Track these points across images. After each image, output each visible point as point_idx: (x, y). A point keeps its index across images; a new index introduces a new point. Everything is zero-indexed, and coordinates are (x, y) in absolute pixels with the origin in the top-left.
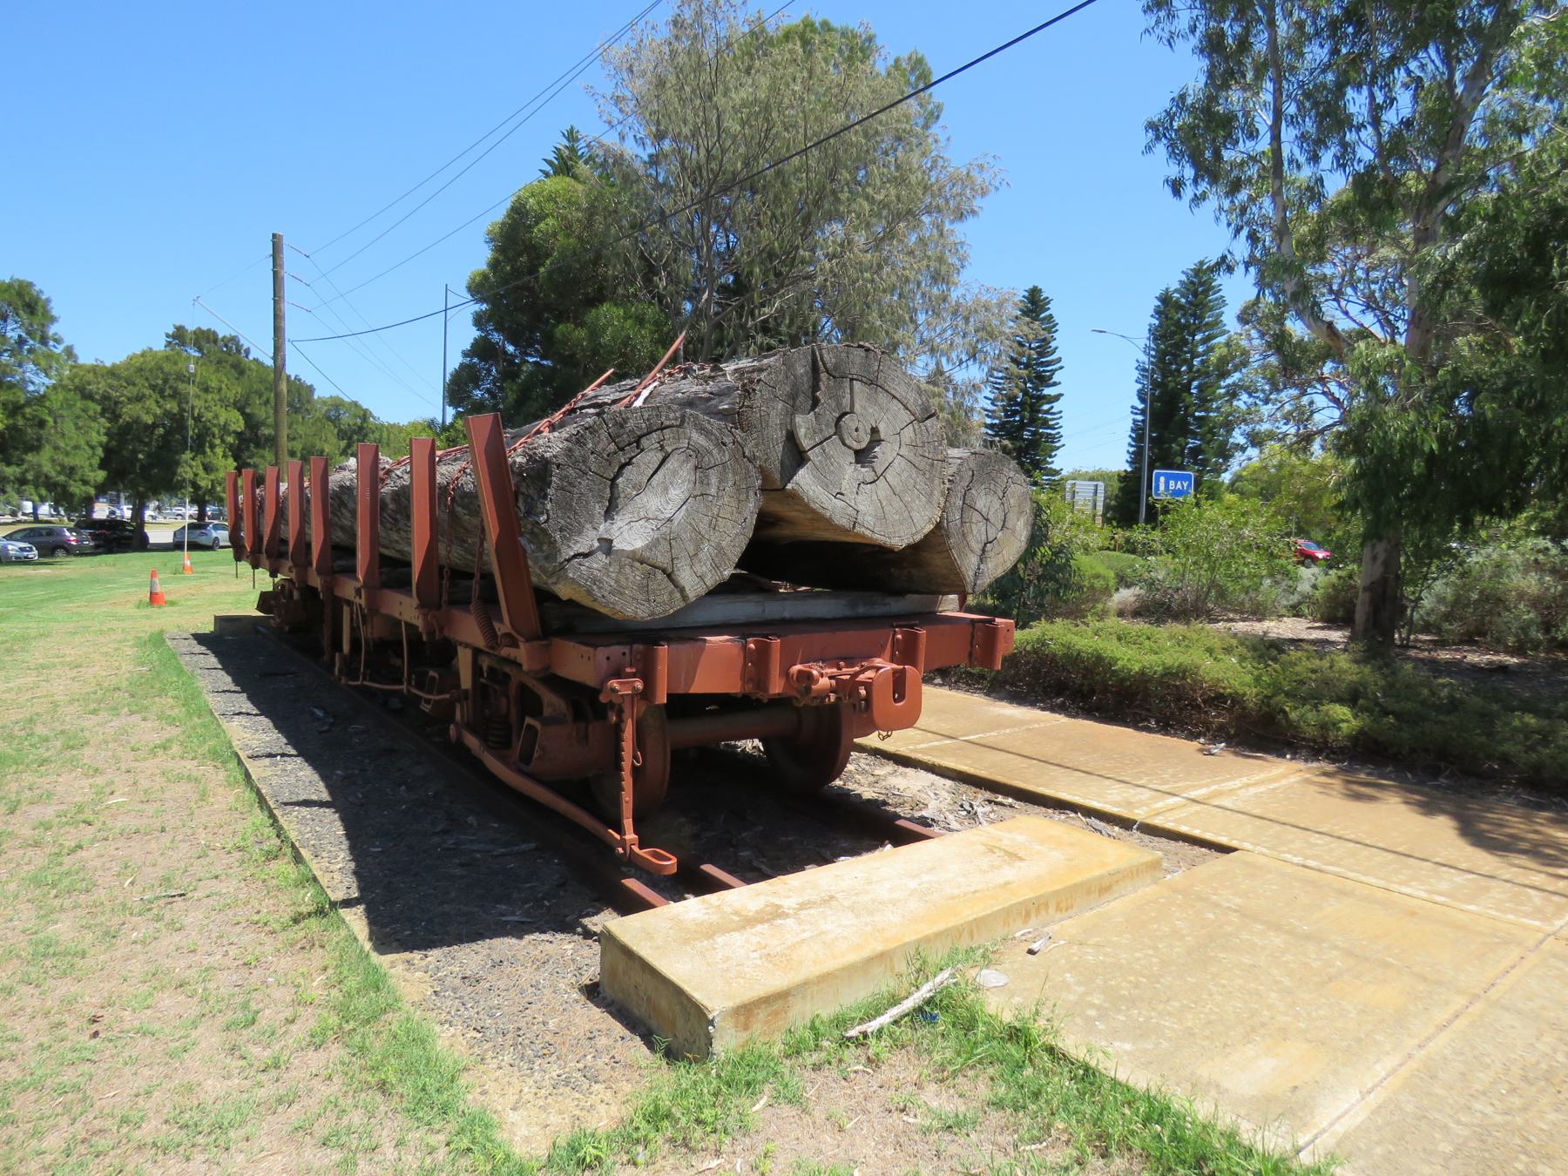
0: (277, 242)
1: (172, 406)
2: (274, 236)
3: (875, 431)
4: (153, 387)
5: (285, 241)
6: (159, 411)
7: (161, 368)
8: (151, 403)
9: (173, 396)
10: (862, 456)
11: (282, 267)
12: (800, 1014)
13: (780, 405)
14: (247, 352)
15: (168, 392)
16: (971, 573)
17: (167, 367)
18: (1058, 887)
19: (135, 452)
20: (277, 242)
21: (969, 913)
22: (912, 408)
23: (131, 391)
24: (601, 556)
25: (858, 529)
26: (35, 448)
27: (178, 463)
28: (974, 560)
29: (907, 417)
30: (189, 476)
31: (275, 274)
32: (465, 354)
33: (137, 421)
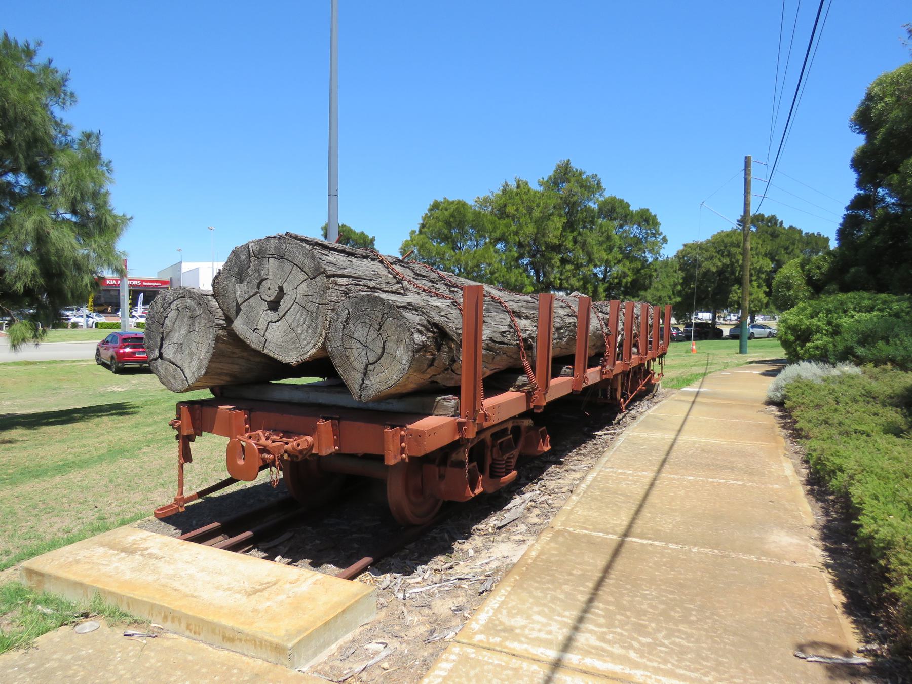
0: (747, 161)
1: (726, 261)
2: (746, 157)
3: (281, 289)
4: (718, 252)
5: (752, 159)
6: (720, 264)
7: (723, 241)
8: (716, 261)
9: (728, 255)
10: (274, 306)
11: (750, 174)
12: (54, 591)
13: (233, 279)
14: (781, 223)
15: (726, 253)
16: (357, 386)
17: (726, 240)
18: (190, 613)
19: (707, 287)
20: (747, 161)
21: (138, 595)
22: (306, 270)
23: (706, 255)
24: (159, 360)
25: (265, 351)
26: (646, 290)
27: (730, 292)
28: (358, 377)
29: (302, 276)
30: (736, 299)
31: (746, 179)
32: (848, 209)
33: (709, 270)
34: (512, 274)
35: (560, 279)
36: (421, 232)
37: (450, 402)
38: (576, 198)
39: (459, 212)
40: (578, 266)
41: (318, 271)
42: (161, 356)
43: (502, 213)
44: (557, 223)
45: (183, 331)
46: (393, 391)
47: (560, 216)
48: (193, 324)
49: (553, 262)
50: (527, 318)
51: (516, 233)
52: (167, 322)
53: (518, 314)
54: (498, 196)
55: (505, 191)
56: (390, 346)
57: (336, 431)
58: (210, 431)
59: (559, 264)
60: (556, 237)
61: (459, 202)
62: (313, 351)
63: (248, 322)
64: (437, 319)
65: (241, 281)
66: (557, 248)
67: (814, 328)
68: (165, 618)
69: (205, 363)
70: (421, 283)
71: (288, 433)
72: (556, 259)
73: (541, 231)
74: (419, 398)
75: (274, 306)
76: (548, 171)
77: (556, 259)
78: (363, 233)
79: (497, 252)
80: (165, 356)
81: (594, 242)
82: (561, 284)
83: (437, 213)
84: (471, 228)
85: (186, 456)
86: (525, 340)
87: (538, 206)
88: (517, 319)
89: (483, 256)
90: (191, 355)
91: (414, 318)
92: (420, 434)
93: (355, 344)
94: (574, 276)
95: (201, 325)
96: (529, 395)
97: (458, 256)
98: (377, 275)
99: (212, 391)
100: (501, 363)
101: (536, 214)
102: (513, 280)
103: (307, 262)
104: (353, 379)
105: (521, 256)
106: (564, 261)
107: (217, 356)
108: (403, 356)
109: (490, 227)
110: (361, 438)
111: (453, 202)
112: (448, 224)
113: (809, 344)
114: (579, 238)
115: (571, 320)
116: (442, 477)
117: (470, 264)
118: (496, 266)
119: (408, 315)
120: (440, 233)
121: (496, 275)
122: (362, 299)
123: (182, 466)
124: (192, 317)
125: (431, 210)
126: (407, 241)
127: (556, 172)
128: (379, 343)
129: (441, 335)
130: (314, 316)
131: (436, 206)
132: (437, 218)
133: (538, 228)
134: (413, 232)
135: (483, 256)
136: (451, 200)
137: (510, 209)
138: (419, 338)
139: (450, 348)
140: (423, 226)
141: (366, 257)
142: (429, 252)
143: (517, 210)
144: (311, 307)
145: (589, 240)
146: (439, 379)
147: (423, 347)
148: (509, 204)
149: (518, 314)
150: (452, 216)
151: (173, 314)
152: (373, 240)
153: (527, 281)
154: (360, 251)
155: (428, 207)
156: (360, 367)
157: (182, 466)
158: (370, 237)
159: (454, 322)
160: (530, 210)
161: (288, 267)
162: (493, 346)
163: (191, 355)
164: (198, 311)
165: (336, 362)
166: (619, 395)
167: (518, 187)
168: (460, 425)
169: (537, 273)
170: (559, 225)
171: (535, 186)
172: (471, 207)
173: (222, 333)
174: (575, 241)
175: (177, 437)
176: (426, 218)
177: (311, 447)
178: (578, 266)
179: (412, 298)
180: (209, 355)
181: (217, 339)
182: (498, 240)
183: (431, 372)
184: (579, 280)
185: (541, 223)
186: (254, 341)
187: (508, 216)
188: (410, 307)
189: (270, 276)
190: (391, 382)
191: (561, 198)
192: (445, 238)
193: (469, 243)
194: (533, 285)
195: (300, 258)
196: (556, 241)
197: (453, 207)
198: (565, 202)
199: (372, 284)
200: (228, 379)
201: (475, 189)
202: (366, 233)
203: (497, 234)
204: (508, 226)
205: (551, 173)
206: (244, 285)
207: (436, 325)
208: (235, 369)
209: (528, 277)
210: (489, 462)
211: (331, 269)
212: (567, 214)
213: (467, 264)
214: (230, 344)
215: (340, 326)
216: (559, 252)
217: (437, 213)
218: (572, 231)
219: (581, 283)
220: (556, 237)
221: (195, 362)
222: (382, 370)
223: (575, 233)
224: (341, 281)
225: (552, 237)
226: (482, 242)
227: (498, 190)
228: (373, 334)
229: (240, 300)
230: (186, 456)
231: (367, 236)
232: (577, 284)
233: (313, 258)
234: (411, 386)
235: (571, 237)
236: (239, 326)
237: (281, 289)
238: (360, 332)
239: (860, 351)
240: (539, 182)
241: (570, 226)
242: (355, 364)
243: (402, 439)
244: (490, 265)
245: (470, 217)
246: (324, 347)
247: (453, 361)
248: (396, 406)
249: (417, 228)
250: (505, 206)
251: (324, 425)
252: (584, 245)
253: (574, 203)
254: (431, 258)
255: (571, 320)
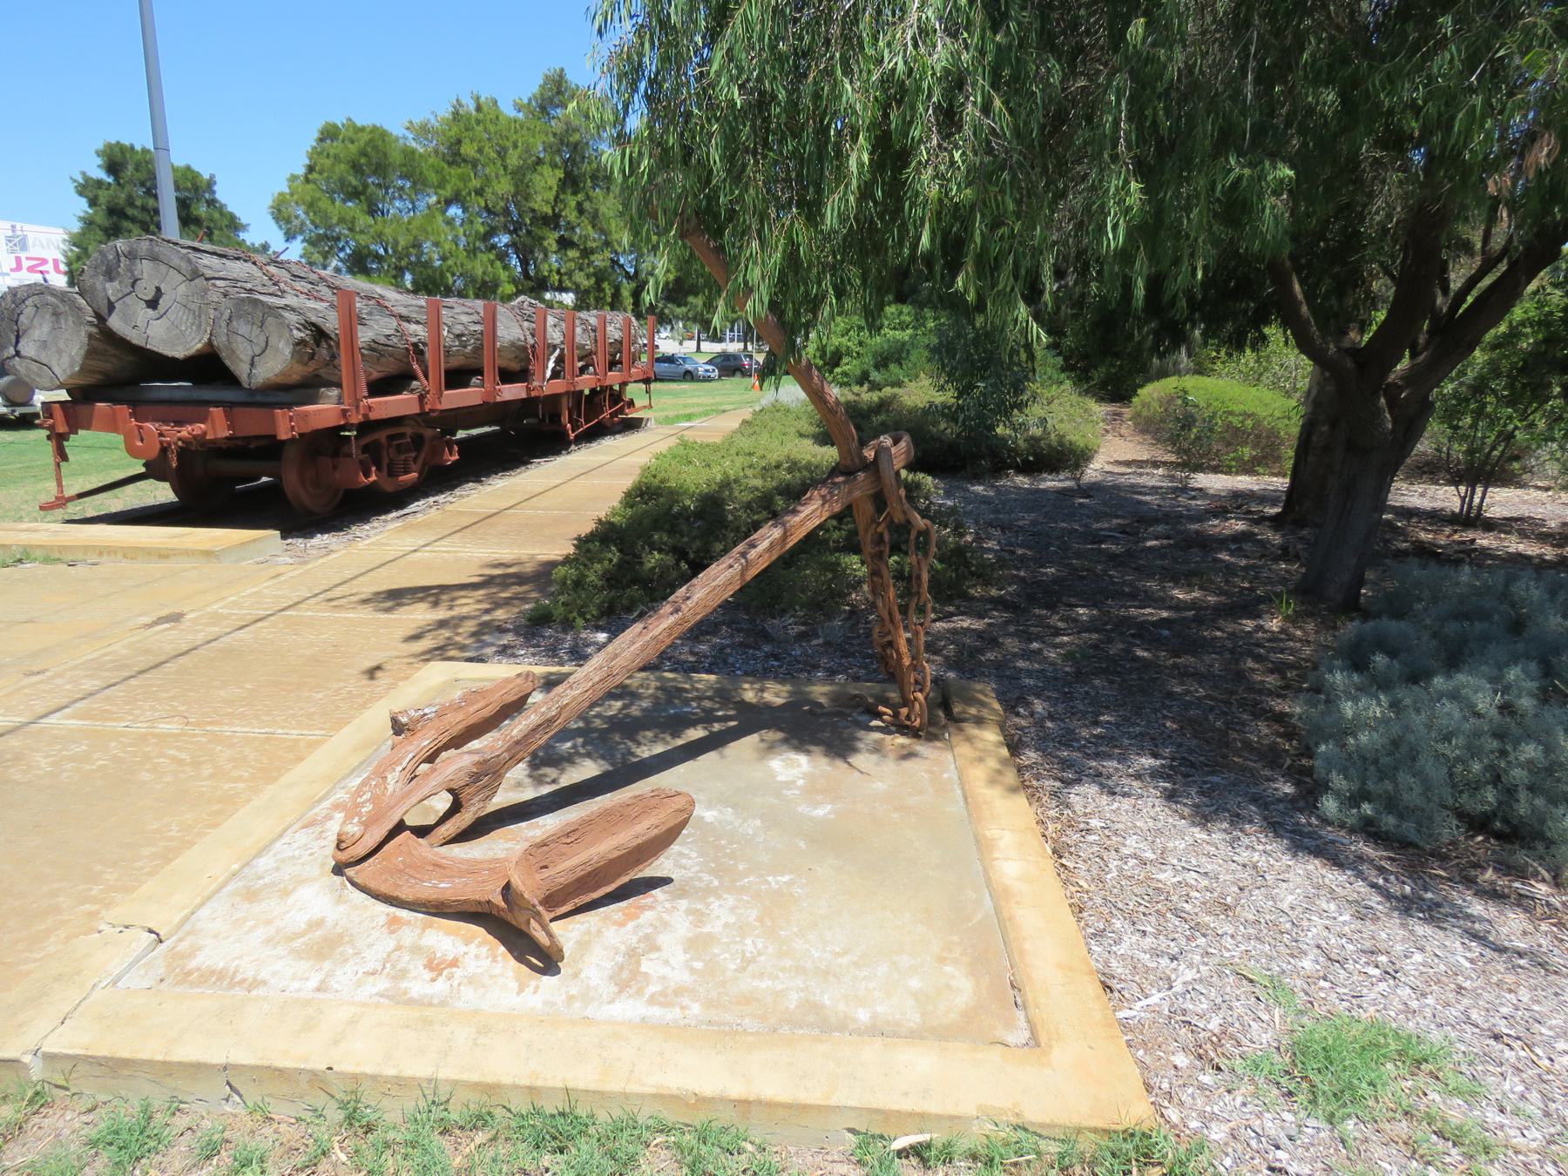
3: (158, 289)
10: (153, 304)
34: (477, 264)
35: (558, 272)
36: (307, 181)
37: (334, 392)
38: (577, 137)
39: (375, 148)
40: (586, 253)
41: (195, 274)
42: (18, 354)
43: (454, 156)
44: (547, 180)
45: (46, 328)
46: (279, 380)
47: (554, 166)
48: (58, 320)
49: (545, 243)
50: (418, 323)
51: (480, 192)
52: (22, 318)
53: (408, 320)
54: (444, 121)
55: (456, 115)
56: (272, 341)
57: (227, 417)
58: (88, 428)
59: (554, 247)
60: (547, 202)
61: (375, 129)
62: (199, 346)
63: (125, 319)
64: (313, 319)
65: (111, 279)
66: (552, 221)
67: (843, 350)
68: (101, 554)
69: (79, 360)
70: (299, 285)
71: (179, 423)
72: (551, 240)
73: (522, 191)
74: (303, 389)
75: (153, 304)
76: (530, 87)
77: (551, 240)
78: (188, 168)
79: (450, 222)
80: (23, 353)
81: (611, 214)
82: (560, 281)
83: (334, 147)
84: (401, 177)
85: (62, 455)
86: (415, 345)
87: (515, 146)
88: (405, 324)
89: (423, 229)
90: (60, 352)
91: (292, 318)
92: (306, 415)
93: (240, 339)
94: (581, 269)
95: (68, 323)
96: (421, 398)
97: (379, 227)
98: (251, 277)
99: (69, 392)
100: (389, 367)
101: (513, 159)
102: (479, 272)
103: (183, 265)
104: (241, 370)
105: (491, 232)
106: (565, 244)
107: (91, 353)
108: (286, 350)
109: (433, 178)
110: (252, 423)
111: (363, 129)
112: (356, 168)
113: (838, 370)
114: (587, 205)
115: (478, 328)
116: (335, 467)
117: (402, 242)
118: (447, 247)
119: (286, 314)
120: (343, 183)
121: (450, 262)
122: (243, 300)
123: (58, 465)
124: (56, 314)
125: (321, 140)
126: (281, 194)
127: (542, 87)
128: (262, 339)
129: (319, 334)
130: (198, 315)
131: (329, 134)
132: (336, 157)
133: (516, 186)
134: (293, 178)
135: (423, 229)
136: (359, 124)
137: (468, 149)
138: (298, 334)
139: (330, 346)
140: (311, 169)
141: (238, 259)
142: (326, 217)
143: (480, 151)
144: (193, 306)
145: (603, 209)
146: (322, 372)
147: (302, 342)
148: (463, 144)
149: (408, 320)
150: (363, 153)
151: (28, 311)
152: (211, 183)
153: (504, 275)
154: (231, 252)
155: (316, 135)
156: (247, 359)
157: (58, 465)
158: (206, 176)
159: (331, 323)
160: (502, 153)
161: (163, 268)
162: (376, 349)
163: (60, 352)
164: (62, 308)
165: (223, 355)
166: (565, 418)
167: (479, 109)
168: (344, 412)
169: (524, 263)
170: (553, 182)
171: (508, 111)
172: (397, 139)
173: (94, 330)
174: (580, 209)
175: (49, 438)
176: (315, 154)
177: (205, 433)
178: (586, 253)
179: (290, 300)
180: (83, 352)
181: (90, 336)
182: (448, 203)
183: (312, 366)
184: (588, 277)
185: (520, 178)
186: (135, 338)
187: (465, 161)
188: (286, 307)
189: (145, 276)
190: (277, 371)
191: (555, 135)
192: (354, 194)
193: (397, 204)
194: (513, 281)
195: (176, 261)
196: (548, 210)
197: (365, 137)
198: (562, 142)
199: (249, 286)
200: (99, 377)
201: (405, 109)
202: (196, 167)
203: (447, 192)
204: (464, 179)
205: (535, 89)
206: (116, 284)
207: (313, 324)
208: (108, 366)
209: (506, 267)
210: (385, 461)
211: (209, 273)
212: (566, 162)
213: (396, 243)
214: (106, 339)
215: (224, 324)
216: (557, 227)
217: (334, 147)
218: (575, 193)
219: (593, 280)
220: (547, 202)
221: (65, 359)
222: (265, 359)
223: (580, 197)
224: (218, 283)
225: (541, 202)
226: (421, 205)
227: (445, 112)
228: (256, 330)
229: (113, 299)
230: (62, 455)
231: (198, 175)
232: (586, 283)
233: (189, 261)
234: (295, 378)
235: (573, 204)
236: (115, 322)
237: (158, 289)
238: (243, 328)
239: (875, 376)
240: (515, 104)
241: (571, 182)
242: (242, 356)
243: (291, 419)
244: (436, 244)
245: (396, 157)
246: (210, 343)
247: (333, 357)
248: (282, 397)
249: (301, 171)
250: (459, 142)
251: (217, 412)
252: (595, 218)
253: (576, 145)
254: (330, 227)
255: (478, 328)
